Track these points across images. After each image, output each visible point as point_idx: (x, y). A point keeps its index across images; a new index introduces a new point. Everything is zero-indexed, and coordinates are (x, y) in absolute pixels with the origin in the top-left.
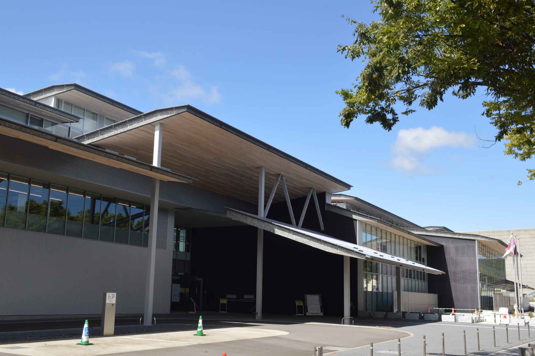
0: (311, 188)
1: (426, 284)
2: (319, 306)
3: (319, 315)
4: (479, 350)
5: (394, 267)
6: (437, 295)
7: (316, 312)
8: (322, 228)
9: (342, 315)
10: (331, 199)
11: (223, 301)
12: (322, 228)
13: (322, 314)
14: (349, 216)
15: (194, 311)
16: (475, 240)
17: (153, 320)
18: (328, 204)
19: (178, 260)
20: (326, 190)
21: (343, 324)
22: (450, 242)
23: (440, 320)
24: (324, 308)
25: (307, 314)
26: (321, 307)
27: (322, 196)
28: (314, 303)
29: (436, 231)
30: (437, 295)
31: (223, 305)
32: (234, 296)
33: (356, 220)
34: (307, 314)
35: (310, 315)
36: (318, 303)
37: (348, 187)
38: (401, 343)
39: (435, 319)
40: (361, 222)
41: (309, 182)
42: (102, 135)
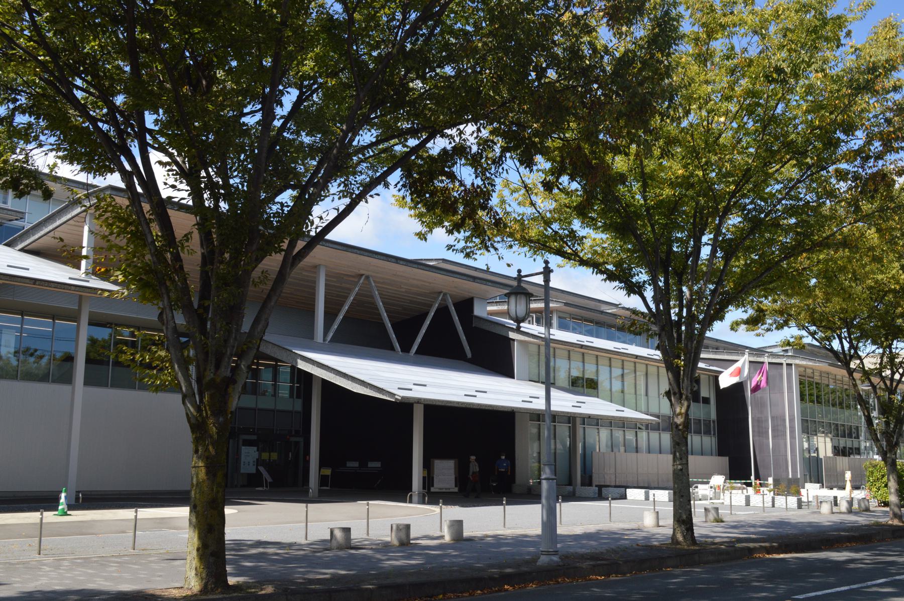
0: (441, 292)
2: (452, 478)
3: (451, 490)
4: (368, 534)
7: (448, 486)
8: (469, 355)
9: (410, 489)
12: (469, 355)
13: (456, 490)
14: (504, 334)
15: (262, 486)
16: (782, 364)
18: (477, 317)
19: (259, 410)
20: (471, 295)
21: (411, 502)
23: (624, 497)
25: (432, 490)
26: (456, 478)
27: (466, 306)
28: (327, 472)
32: (356, 464)
33: (514, 340)
34: (432, 490)
35: (437, 490)
36: (452, 471)
39: (592, 495)
40: (520, 342)
42: (22, 242)
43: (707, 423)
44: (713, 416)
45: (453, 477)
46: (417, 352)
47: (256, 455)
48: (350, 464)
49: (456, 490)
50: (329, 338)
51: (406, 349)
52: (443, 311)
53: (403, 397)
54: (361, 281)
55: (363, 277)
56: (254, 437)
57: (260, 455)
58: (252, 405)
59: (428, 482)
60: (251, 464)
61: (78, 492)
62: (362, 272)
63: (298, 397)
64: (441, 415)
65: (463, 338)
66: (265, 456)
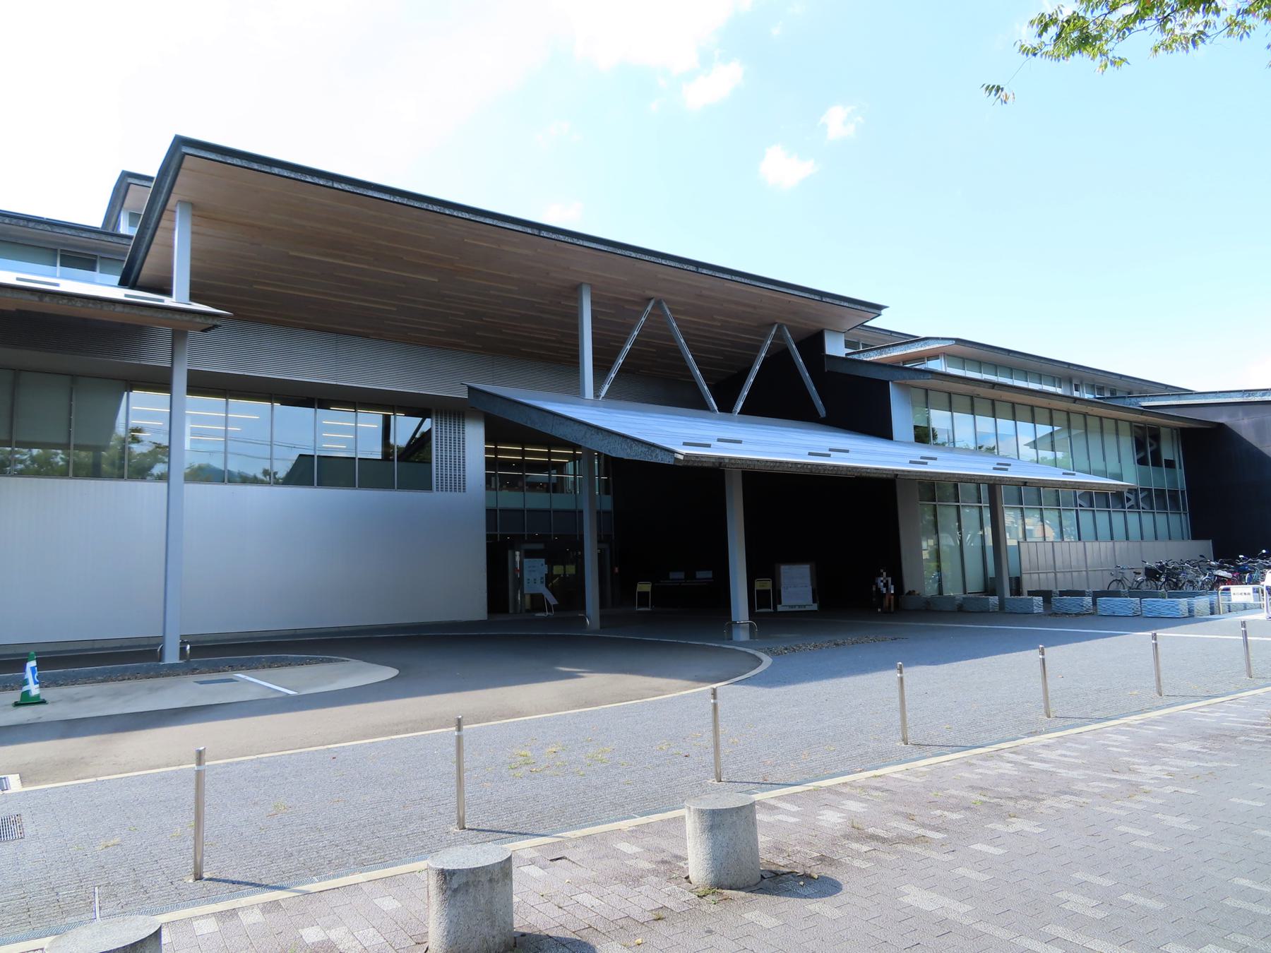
1: (1185, 519)
3: (808, 608)
5: (973, 486)
6: (1210, 542)
8: (822, 412)
10: (835, 347)
11: (644, 587)
12: (822, 412)
13: (815, 607)
17: (183, 650)
20: (820, 326)
22: (1240, 414)
24: (820, 593)
25: (780, 608)
27: (813, 343)
29: (964, 361)
30: (1210, 542)
31: (643, 595)
32: (681, 575)
34: (780, 608)
37: (877, 309)
38: (719, 702)
41: (749, 310)
43: (1174, 494)
44: (1181, 484)
45: (809, 589)
46: (742, 412)
47: (545, 569)
48: (673, 575)
49: (815, 607)
50: (603, 394)
51: (657, 317)
52: (779, 358)
53: (686, 456)
54: (649, 308)
55: (652, 303)
56: (540, 546)
57: (550, 570)
58: (519, 505)
59: (763, 603)
60: (538, 581)
61: (183, 643)
62: (649, 293)
63: (607, 493)
64: (766, 483)
65: (812, 389)
66: (558, 570)
